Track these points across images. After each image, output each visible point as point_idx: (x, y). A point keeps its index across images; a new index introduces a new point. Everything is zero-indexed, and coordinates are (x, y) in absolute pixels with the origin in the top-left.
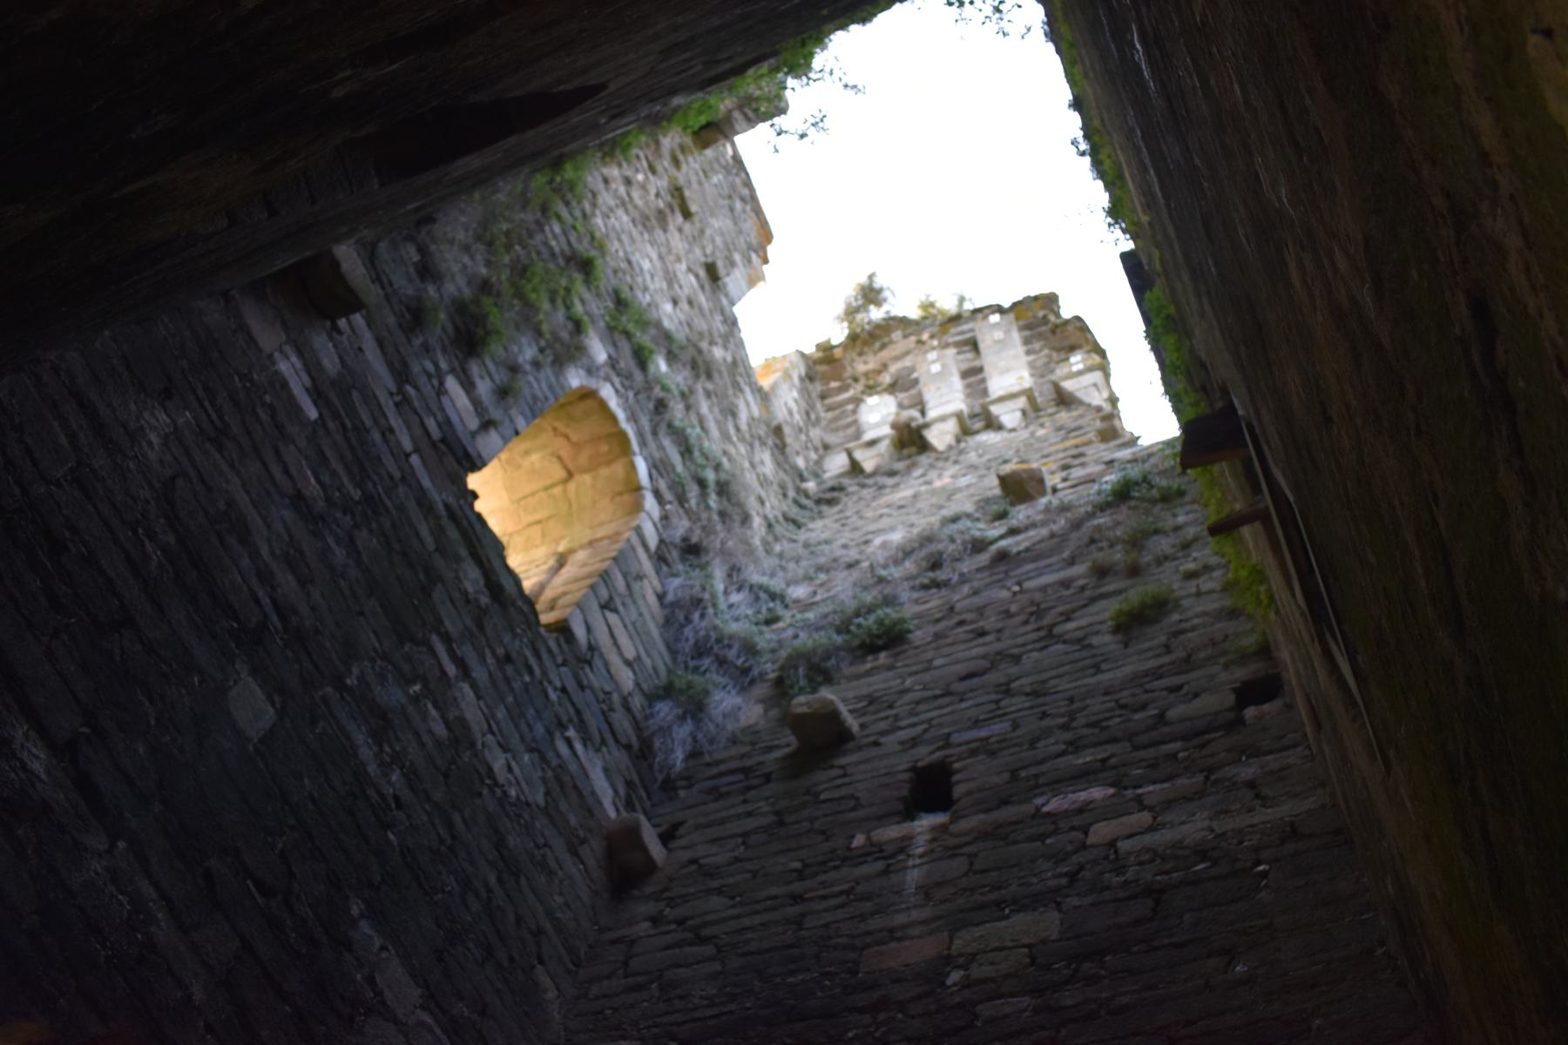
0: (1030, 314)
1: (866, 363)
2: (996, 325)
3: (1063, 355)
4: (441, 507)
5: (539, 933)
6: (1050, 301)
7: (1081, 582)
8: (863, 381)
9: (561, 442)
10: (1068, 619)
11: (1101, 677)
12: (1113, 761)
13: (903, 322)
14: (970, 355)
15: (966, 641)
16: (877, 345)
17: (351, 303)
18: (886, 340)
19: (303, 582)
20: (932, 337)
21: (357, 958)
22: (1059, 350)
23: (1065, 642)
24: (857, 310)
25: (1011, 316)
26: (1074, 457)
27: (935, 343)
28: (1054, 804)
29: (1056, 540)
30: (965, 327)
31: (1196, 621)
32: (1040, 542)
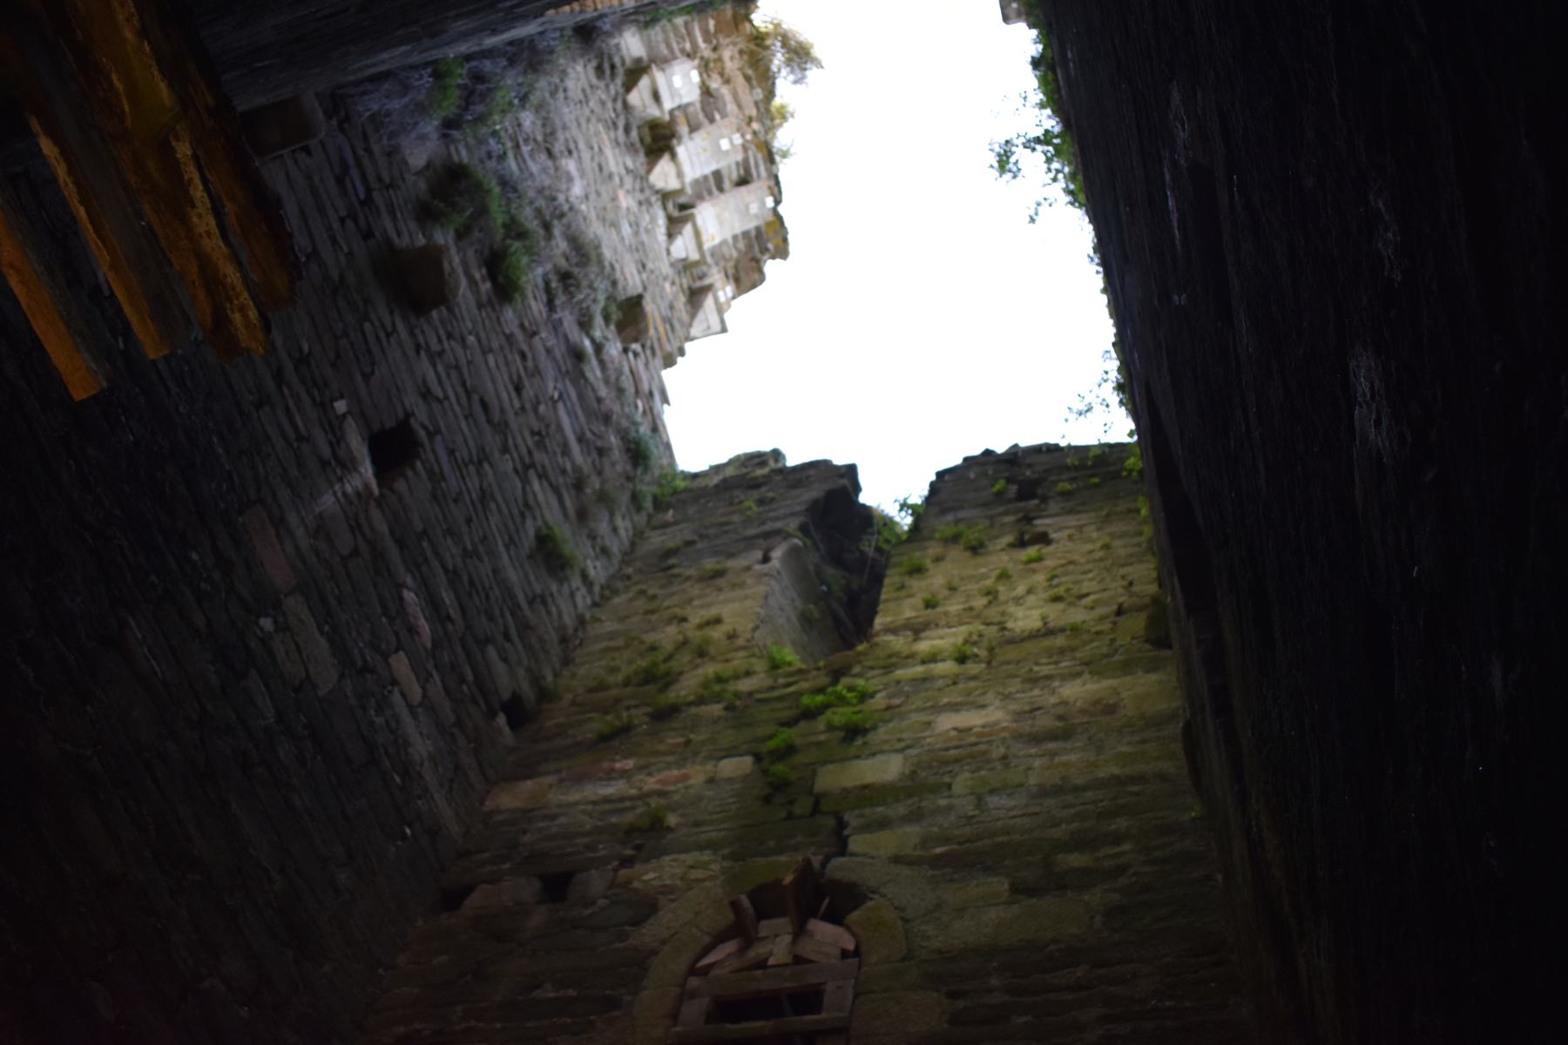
0: (771, 234)
1: (732, 58)
2: (763, 204)
3: (731, 272)
6: (782, 252)
7: (568, 466)
8: (713, 56)
10: (540, 477)
11: (501, 548)
12: (450, 626)
13: (770, 94)
14: (735, 176)
15: (511, 378)
16: (749, 72)
18: (754, 83)
20: (755, 133)
22: (736, 267)
23: (524, 489)
24: (785, 44)
25: (771, 218)
26: (652, 348)
27: (749, 137)
28: (409, 596)
29: (595, 405)
30: (762, 168)
31: (554, 610)
32: (593, 390)
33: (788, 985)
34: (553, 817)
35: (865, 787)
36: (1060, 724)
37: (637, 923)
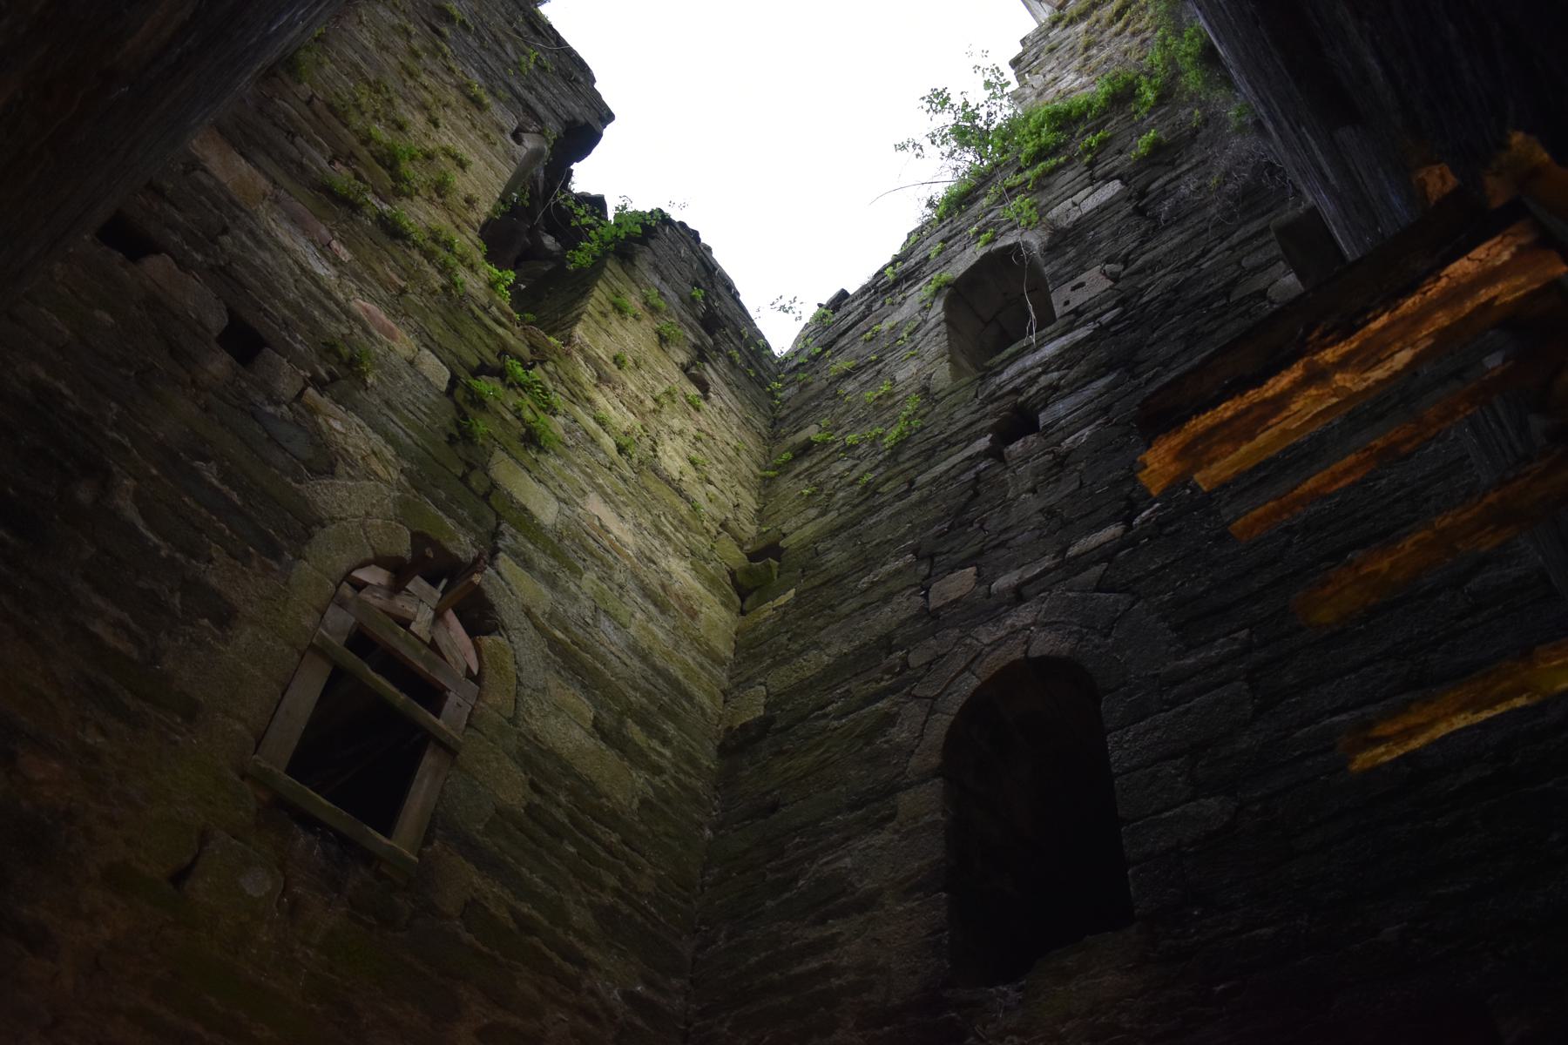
33: (421, 665)
34: (260, 243)
35: (525, 509)
36: (660, 591)
37: (317, 473)
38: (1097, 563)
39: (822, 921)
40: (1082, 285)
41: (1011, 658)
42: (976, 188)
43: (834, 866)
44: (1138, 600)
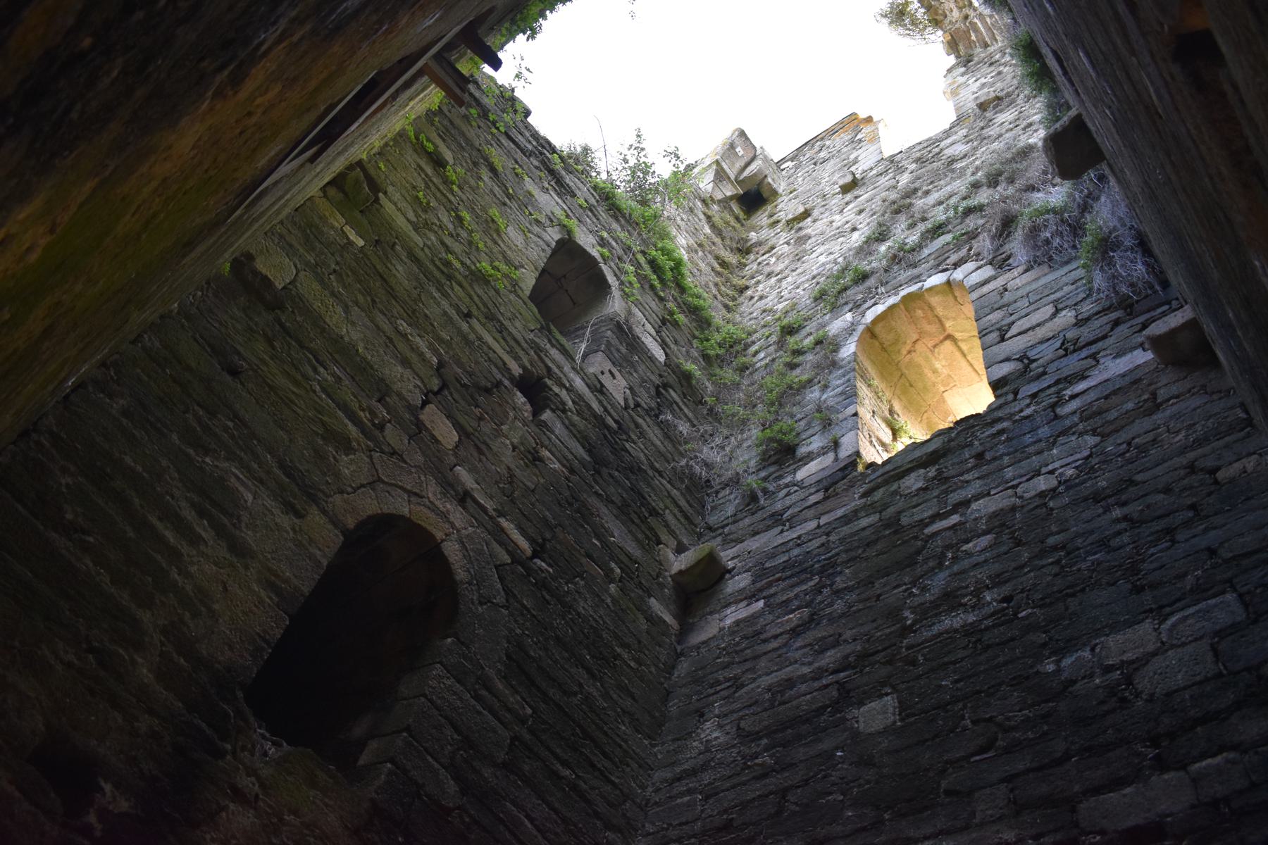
4: (864, 500)
5: (1192, 468)
9: (919, 346)
17: (711, 560)
19: (836, 644)
21: (1083, 678)
38: (509, 552)
39: (202, 513)
40: (614, 377)
41: (434, 531)
42: (624, 216)
43: (241, 489)
44: (507, 608)
